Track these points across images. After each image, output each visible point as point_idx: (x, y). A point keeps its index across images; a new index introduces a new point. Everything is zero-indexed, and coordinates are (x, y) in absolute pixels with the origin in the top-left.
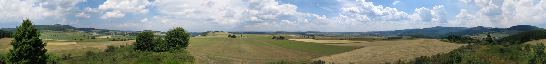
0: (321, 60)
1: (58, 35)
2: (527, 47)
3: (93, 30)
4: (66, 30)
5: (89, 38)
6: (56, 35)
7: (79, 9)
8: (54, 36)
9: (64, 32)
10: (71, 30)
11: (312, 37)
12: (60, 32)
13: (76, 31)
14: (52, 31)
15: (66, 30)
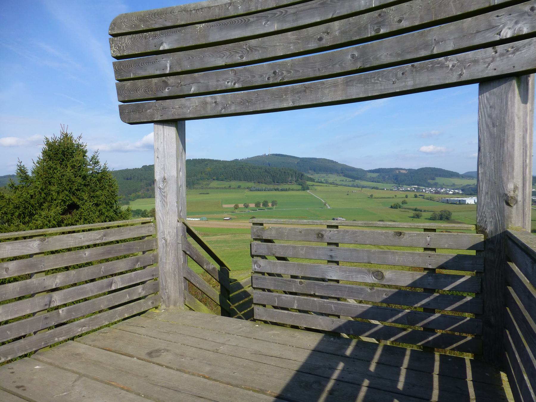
0: (22, 171)
1: (274, 203)
2: (13, 186)
3: (440, 180)
4: (312, 180)
5: (418, 216)
6: (265, 204)
7: (59, 340)
8: (257, 205)
9: (305, 188)
10: (333, 178)
11: (422, 197)
12: (87, 226)
13: (358, 182)
14: (251, 184)
15: (312, 180)
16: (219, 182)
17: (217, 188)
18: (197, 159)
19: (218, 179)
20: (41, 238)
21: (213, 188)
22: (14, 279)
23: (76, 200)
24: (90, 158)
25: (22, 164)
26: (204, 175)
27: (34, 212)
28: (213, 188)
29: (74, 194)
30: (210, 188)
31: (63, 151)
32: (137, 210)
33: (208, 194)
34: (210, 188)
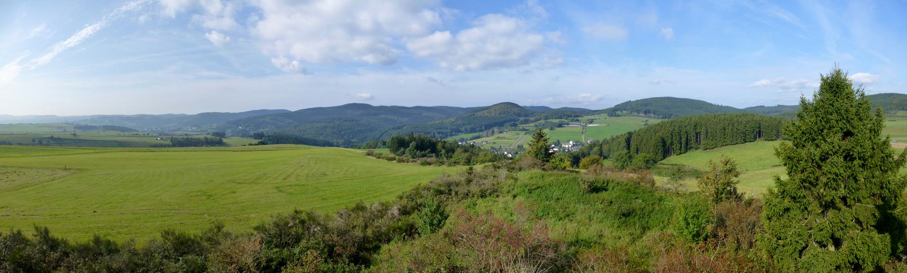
0: (803, 101)
16: (904, 112)
17: (903, 117)
18: (883, 93)
19: (903, 110)
20: (432, 80)
21: (900, 117)
22: (697, 178)
23: (851, 129)
24: (856, 92)
25: (804, 97)
26: (892, 106)
27: (816, 138)
28: (900, 117)
29: (849, 122)
30: (897, 116)
31: (837, 85)
32: (616, 106)
33: (895, 121)
34: (897, 116)
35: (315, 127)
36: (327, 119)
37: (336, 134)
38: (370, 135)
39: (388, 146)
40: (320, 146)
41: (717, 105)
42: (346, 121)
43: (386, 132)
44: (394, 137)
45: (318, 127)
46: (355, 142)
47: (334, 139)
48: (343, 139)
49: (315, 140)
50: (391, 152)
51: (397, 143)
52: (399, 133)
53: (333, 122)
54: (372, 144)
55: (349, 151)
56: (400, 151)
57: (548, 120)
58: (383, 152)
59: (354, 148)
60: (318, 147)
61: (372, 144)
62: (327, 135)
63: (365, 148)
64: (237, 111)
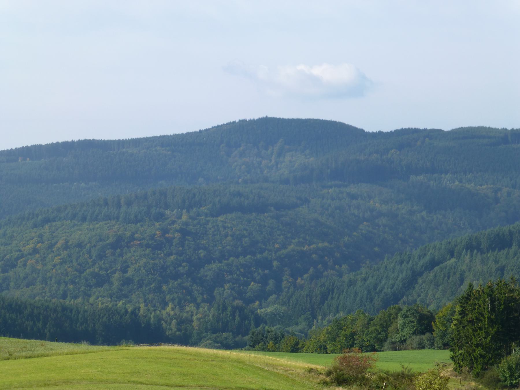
0: (254, 119)
35: (66, 247)
36: (129, 204)
37: (176, 276)
38: (351, 283)
39: (444, 335)
40: (93, 342)
41: (194, 131)
42: (226, 209)
43: (433, 264)
44: (476, 288)
45: (80, 245)
46: (274, 318)
47: (165, 304)
48: (210, 300)
49: (64, 309)
50: (458, 369)
51: (492, 322)
52: (502, 270)
53: (160, 217)
54: (358, 327)
55: (238, 361)
56: (504, 365)
57: (269, 300)
58: (415, 368)
59: (263, 349)
60: (84, 347)
61: (358, 327)
62: (128, 282)
63: (323, 349)
64: (196, 128)
